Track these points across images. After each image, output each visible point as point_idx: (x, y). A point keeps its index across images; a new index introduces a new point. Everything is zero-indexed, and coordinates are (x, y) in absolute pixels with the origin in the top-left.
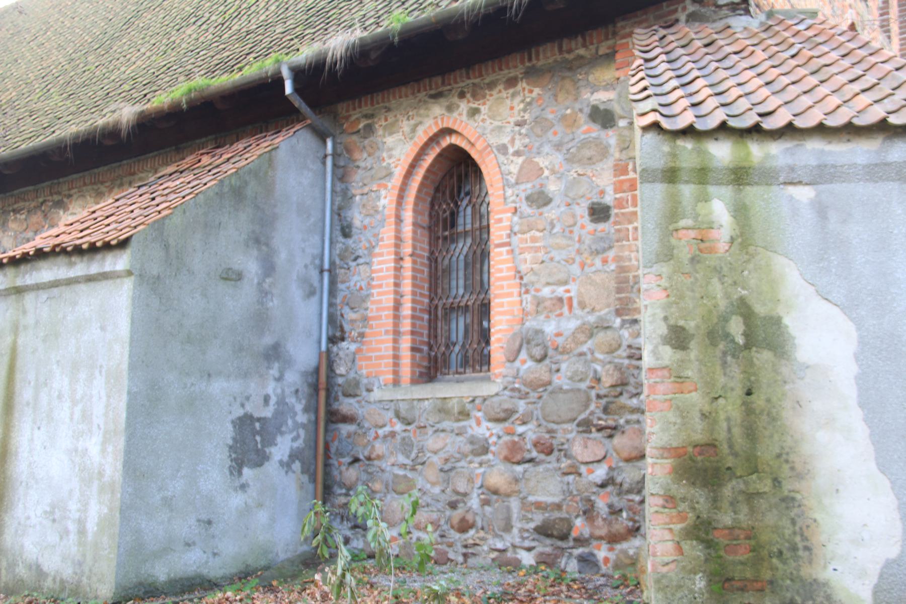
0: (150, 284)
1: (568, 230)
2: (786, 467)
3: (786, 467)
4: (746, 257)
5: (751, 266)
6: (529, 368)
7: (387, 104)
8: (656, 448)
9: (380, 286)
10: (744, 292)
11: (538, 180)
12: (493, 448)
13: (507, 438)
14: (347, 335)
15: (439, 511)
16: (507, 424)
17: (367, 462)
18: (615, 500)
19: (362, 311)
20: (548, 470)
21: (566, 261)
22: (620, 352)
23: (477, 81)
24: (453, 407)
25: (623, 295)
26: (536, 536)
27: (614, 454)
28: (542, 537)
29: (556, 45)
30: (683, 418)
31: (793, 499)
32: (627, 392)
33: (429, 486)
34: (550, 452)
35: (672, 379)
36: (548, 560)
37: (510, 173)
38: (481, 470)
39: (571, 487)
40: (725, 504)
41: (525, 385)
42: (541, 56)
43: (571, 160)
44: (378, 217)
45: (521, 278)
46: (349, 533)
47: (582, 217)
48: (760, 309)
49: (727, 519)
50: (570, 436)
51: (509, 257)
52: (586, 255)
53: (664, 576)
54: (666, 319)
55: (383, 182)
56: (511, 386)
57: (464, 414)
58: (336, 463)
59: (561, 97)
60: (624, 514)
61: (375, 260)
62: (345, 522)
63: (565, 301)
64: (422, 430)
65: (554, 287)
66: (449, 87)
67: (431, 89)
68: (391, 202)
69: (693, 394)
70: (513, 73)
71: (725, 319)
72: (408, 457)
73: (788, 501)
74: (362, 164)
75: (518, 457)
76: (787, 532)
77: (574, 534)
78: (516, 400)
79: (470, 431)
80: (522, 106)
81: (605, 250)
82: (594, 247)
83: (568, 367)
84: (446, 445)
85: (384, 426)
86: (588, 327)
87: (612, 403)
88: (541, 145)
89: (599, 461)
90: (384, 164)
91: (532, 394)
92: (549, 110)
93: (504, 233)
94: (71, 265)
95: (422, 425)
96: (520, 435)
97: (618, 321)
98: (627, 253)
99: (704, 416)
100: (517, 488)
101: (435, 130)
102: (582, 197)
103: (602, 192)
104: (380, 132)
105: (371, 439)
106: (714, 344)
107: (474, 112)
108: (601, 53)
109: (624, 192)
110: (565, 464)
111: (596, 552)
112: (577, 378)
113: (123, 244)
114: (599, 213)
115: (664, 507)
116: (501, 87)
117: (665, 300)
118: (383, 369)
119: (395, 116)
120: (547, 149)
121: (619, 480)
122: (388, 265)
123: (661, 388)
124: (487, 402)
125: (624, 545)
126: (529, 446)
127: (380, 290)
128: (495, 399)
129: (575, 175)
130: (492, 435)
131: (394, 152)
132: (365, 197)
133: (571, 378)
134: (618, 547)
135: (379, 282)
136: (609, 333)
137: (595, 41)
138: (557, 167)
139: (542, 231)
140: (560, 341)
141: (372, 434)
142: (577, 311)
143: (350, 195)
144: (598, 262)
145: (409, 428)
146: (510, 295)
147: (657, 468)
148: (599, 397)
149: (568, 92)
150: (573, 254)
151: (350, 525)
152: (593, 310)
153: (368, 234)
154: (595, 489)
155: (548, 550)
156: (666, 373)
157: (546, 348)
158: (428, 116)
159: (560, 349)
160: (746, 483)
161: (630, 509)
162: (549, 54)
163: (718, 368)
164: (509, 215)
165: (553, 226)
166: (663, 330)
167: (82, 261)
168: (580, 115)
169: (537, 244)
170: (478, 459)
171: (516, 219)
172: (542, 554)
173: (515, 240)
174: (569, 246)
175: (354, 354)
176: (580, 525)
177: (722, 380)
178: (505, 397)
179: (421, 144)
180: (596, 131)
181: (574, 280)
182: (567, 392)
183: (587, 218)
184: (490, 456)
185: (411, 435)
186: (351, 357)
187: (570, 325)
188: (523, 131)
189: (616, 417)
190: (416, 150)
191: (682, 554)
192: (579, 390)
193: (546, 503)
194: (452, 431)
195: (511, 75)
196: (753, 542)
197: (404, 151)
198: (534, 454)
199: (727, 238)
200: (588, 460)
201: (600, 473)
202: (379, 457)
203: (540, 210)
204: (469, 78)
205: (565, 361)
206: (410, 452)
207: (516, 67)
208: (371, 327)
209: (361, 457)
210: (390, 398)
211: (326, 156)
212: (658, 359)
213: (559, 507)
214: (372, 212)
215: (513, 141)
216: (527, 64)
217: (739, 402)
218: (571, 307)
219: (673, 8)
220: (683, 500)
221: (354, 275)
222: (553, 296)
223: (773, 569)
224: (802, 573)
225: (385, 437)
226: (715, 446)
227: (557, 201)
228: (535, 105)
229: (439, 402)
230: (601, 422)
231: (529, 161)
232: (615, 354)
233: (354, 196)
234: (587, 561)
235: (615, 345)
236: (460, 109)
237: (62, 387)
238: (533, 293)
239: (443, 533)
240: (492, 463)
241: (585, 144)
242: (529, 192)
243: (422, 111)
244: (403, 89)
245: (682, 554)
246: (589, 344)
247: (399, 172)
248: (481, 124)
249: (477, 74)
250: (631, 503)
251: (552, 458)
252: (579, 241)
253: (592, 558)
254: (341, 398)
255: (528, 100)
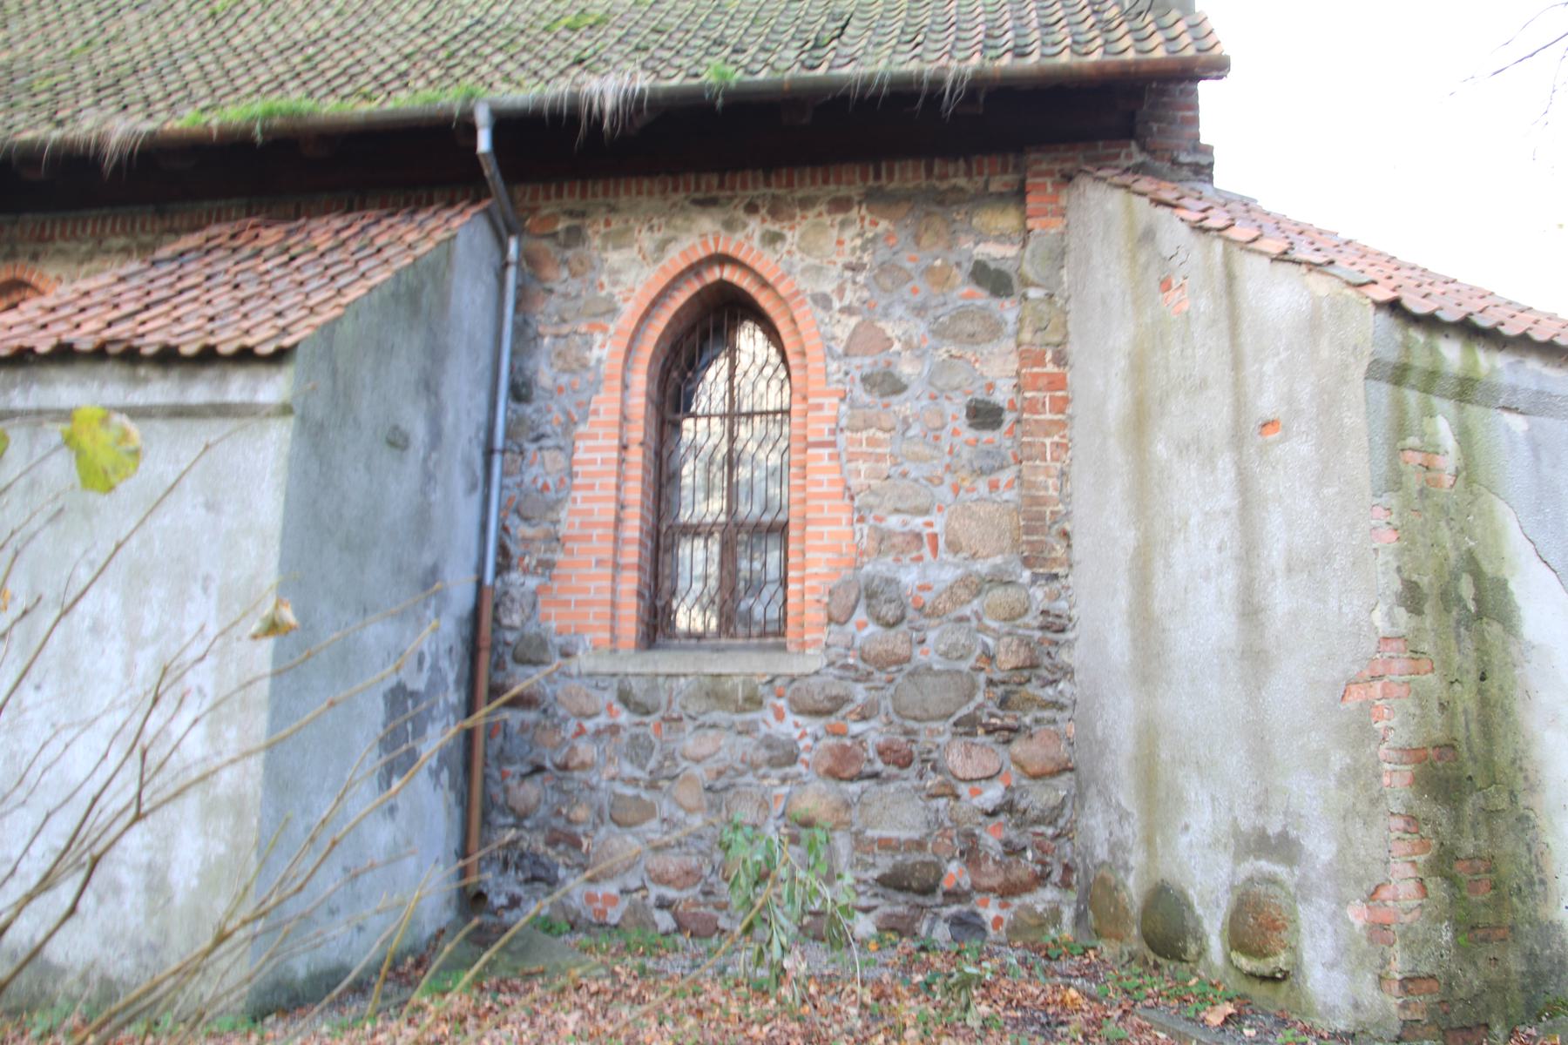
0: (317, 437)
1: (933, 435)
2: (1520, 776)
3: (1520, 776)
4: (1471, 498)
5: (1475, 510)
6: (872, 634)
7: (612, 201)
8: (1394, 749)
9: (591, 487)
10: (1472, 543)
11: (883, 355)
12: (805, 756)
13: (832, 741)
14: (515, 561)
15: (701, 852)
16: (832, 720)
17: (560, 774)
18: (1012, 834)
19: (546, 525)
20: (903, 790)
21: (930, 480)
22: (1028, 619)
23: (781, 192)
24: (734, 689)
25: (1035, 538)
26: (880, 890)
27: (1013, 768)
28: (890, 892)
29: (923, 164)
30: (1422, 707)
31: (1528, 818)
32: (1039, 677)
33: (681, 814)
34: (905, 762)
35: (1408, 654)
36: (899, 926)
37: (833, 338)
38: (785, 790)
39: (941, 816)
40: (1467, 827)
41: (864, 660)
42: (897, 176)
43: (940, 333)
44: (589, 376)
45: (852, 498)
46: (518, 890)
47: (954, 418)
48: (1488, 568)
49: (1468, 846)
50: (942, 740)
51: (834, 463)
52: (963, 473)
53: (1409, 928)
54: (1399, 570)
55: (601, 321)
56: (840, 662)
57: (754, 701)
58: (497, 774)
59: (926, 240)
60: (1029, 854)
61: (580, 444)
62: (512, 872)
63: (925, 539)
64: (674, 725)
65: (907, 517)
66: (728, 193)
67: (698, 188)
68: (613, 355)
69: (1430, 675)
70: (844, 191)
71: (1457, 578)
72: (642, 767)
73: (1523, 819)
74: (559, 288)
75: (853, 770)
76: (1525, 861)
77: (945, 885)
78: (849, 683)
79: (764, 729)
80: (858, 242)
81: (992, 470)
82: (976, 465)
83: (941, 635)
84: (719, 749)
85: (596, 714)
86: (977, 580)
87: (1014, 692)
88: (890, 305)
89: (989, 778)
90: (603, 293)
91: (877, 675)
92: (904, 255)
93: (826, 427)
94: (136, 382)
95: (675, 715)
96: (854, 737)
97: (1026, 575)
98: (1041, 478)
99: (1442, 707)
100: (847, 818)
101: (702, 253)
102: (957, 389)
103: (991, 387)
104: (597, 242)
105: (569, 735)
106: (1447, 610)
107: (773, 239)
108: (993, 188)
109: (1039, 390)
110: (932, 781)
111: (980, 910)
112: (955, 654)
113: (280, 356)
114: (984, 415)
115: (1406, 832)
116: (823, 208)
117: (1396, 545)
118: (591, 621)
119: (627, 221)
120: (898, 311)
121: (1023, 804)
122: (606, 455)
123: (1396, 665)
124: (796, 684)
125: (1028, 899)
126: (872, 754)
127: (589, 494)
128: (812, 680)
129: (945, 356)
130: (803, 735)
131: (623, 278)
132: (562, 342)
133: (945, 655)
134: (1016, 902)
135: (587, 481)
136: (1011, 590)
137: (986, 171)
138: (915, 340)
139: (889, 431)
140: (927, 597)
141: (572, 726)
142: (944, 554)
143: (530, 332)
144: (982, 486)
145: (646, 719)
146: (837, 522)
147: (1396, 776)
148: (991, 683)
149: (938, 234)
150: (940, 471)
151: (521, 876)
152: (974, 556)
153: (567, 401)
154: (981, 819)
155: (901, 909)
156: (1400, 644)
157: (903, 607)
158: (688, 230)
159: (927, 610)
160: (1486, 797)
161: (1039, 846)
162: (910, 175)
163: (1453, 641)
164: (835, 400)
165: (907, 425)
166: (1397, 586)
167: (165, 377)
168: (955, 271)
169: (879, 450)
170: (776, 774)
171: (844, 408)
172: (890, 916)
173: (842, 439)
174: (932, 458)
175: (536, 593)
176: (955, 872)
177: (1457, 658)
178: (831, 678)
179: (675, 271)
180: (982, 298)
181: (940, 509)
182: (939, 674)
183: (962, 421)
184: (799, 768)
185: (650, 731)
186: (530, 599)
187: (945, 574)
188: (861, 278)
189: (1018, 714)
190: (665, 280)
191: (1426, 896)
192: (959, 672)
193: (898, 840)
194: (730, 728)
195: (840, 194)
196: (1494, 876)
197: (642, 277)
198: (879, 765)
199: (1452, 470)
200: (968, 776)
201: (993, 794)
202: (583, 766)
203: (886, 400)
204: (768, 184)
205: (934, 627)
206: (647, 759)
207: (850, 183)
208: (571, 552)
209: (548, 764)
210: (612, 670)
211: (505, 265)
212: (1393, 625)
213: (920, 845)
214: (575, 366)
215: (841, 291)
216: (871, 182)
217: (1474, 689)
218: (935, 550)
219: (1113, 151)
220: (1426, 821)
221: (532, 464)
222: (906, 529)
223: (1514, 910)
224: (1539, 914)
225: (598, 733)
226: (1453, 747)
227: (915, 389)
228: (880, 244)
229: (707, 681)
230: (993, 721)
231: (867, 325)
232: (1018, 622)
233: (542, 336)
234: (967, 925)
235: (1019, 608)
236: (749, 230)
237: (103, 610)
238: (871, 522)
239: (707, 889)
240: (805, 779)
241: (962, 314)
242: (867, 370)
243: (678, 221)
244: (646, 183)
245: (1426, 896)
246: (976, 603)
247: (629, 312)
248: (785, 257)
249: (784, 181)
250: (1038, 839)
251: (911, 772)
252: (951, 452)
253: (972, 919)
254: (510, 665)
255: (870, 235)
